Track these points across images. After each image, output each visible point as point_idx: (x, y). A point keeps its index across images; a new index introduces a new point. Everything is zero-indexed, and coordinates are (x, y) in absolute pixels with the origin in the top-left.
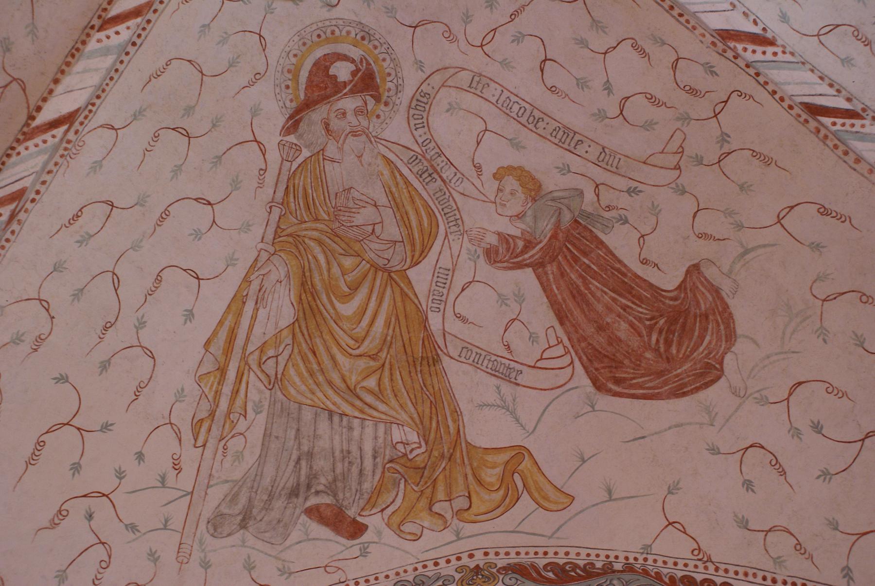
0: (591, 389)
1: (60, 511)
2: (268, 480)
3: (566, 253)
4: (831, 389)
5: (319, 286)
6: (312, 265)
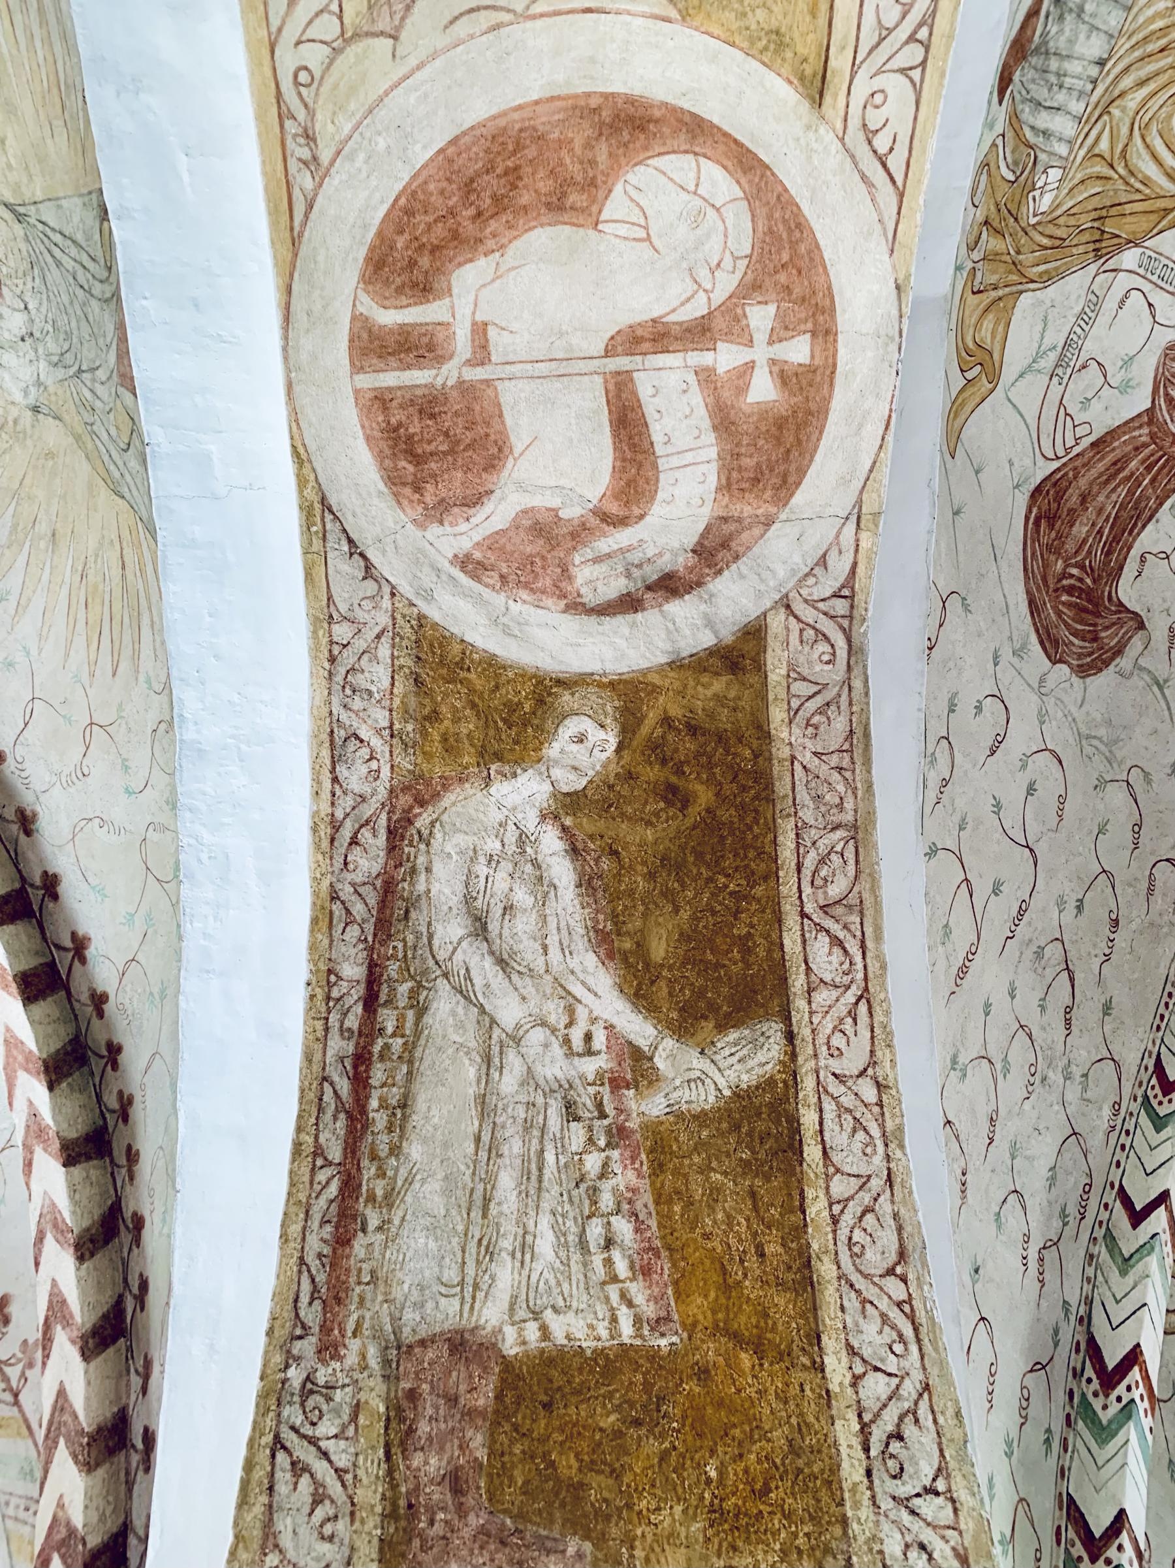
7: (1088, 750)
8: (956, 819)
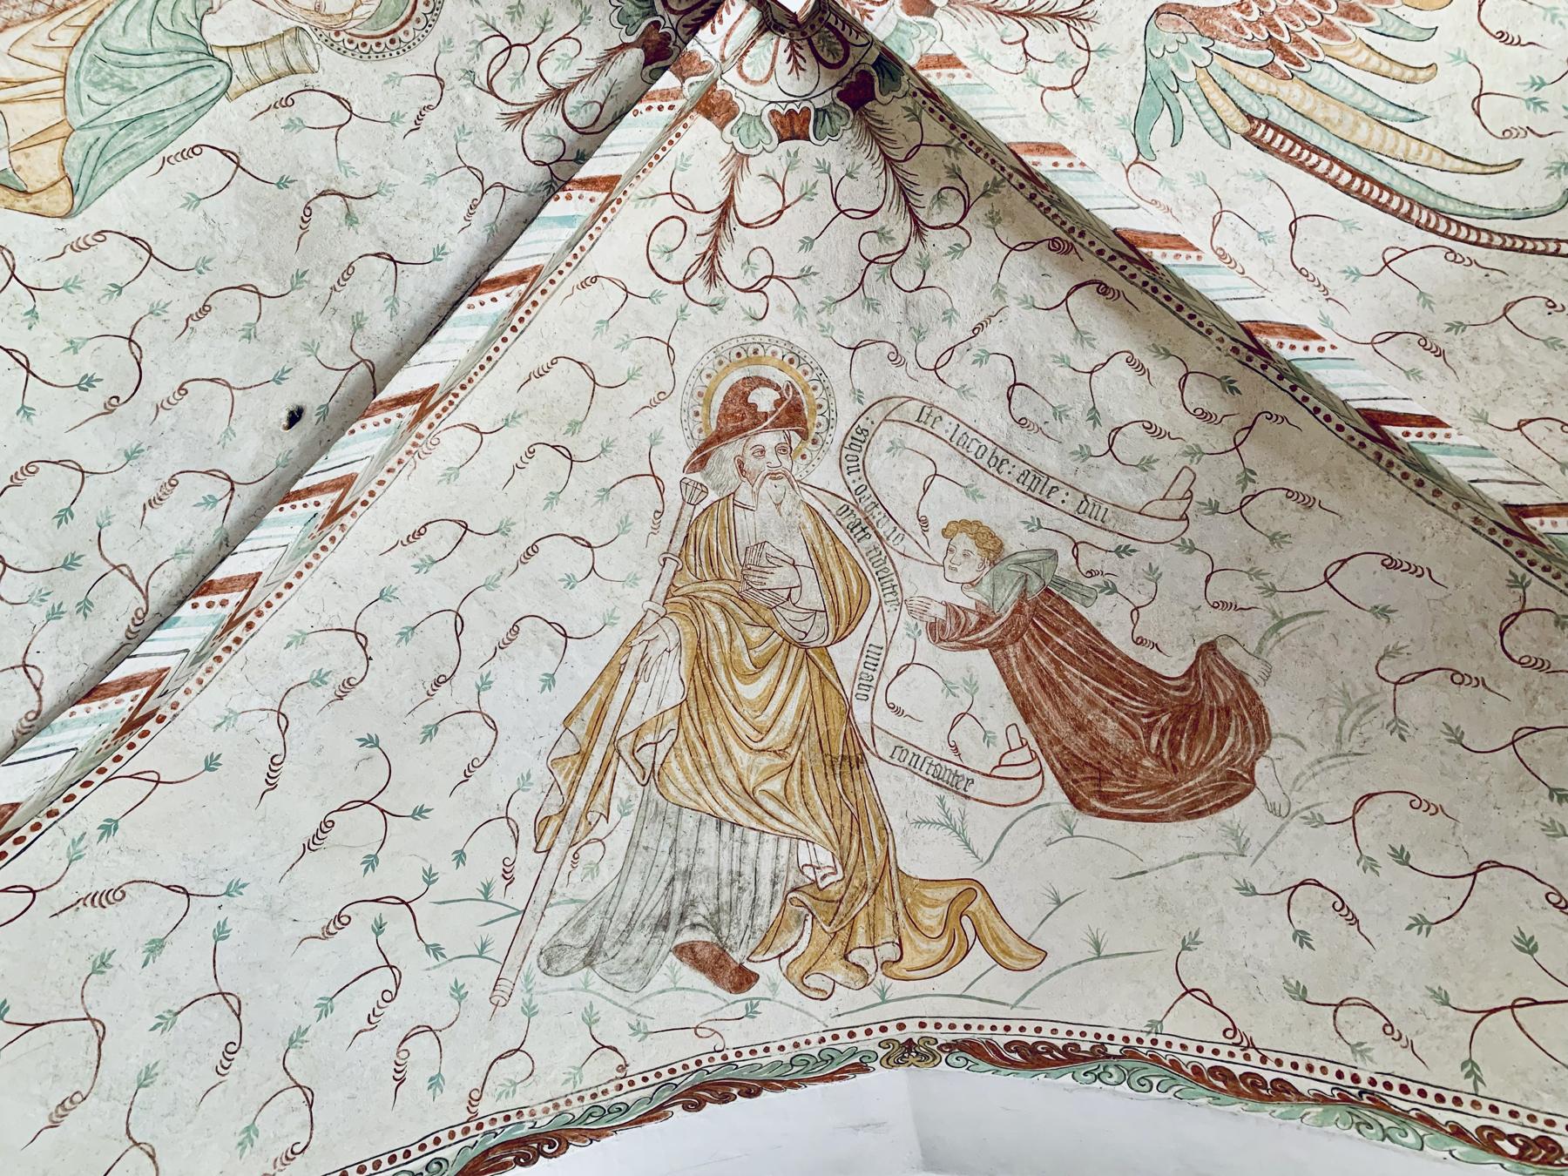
0: (1069, 807)
1: (339, 917)
2: (629, 904)
3: (1035, 628)
4: (1417, 803)
5: (717, 660)
6: (711, 636)
7: (1353, 744)
8: (1433, 1008)
